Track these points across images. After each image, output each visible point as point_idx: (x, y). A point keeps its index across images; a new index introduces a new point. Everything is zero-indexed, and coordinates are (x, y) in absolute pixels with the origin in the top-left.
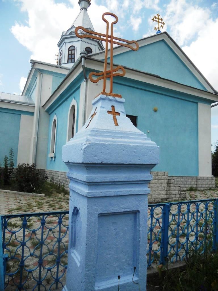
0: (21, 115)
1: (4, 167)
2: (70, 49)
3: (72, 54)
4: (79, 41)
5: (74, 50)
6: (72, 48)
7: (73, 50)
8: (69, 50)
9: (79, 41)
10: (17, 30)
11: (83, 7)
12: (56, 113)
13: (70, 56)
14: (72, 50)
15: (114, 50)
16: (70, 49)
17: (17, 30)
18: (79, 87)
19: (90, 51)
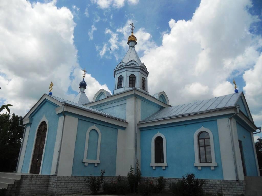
4: (125, 71)
5: (135, 77)
7: (134, 77)
9: (125, 71)
19: (144, 80)
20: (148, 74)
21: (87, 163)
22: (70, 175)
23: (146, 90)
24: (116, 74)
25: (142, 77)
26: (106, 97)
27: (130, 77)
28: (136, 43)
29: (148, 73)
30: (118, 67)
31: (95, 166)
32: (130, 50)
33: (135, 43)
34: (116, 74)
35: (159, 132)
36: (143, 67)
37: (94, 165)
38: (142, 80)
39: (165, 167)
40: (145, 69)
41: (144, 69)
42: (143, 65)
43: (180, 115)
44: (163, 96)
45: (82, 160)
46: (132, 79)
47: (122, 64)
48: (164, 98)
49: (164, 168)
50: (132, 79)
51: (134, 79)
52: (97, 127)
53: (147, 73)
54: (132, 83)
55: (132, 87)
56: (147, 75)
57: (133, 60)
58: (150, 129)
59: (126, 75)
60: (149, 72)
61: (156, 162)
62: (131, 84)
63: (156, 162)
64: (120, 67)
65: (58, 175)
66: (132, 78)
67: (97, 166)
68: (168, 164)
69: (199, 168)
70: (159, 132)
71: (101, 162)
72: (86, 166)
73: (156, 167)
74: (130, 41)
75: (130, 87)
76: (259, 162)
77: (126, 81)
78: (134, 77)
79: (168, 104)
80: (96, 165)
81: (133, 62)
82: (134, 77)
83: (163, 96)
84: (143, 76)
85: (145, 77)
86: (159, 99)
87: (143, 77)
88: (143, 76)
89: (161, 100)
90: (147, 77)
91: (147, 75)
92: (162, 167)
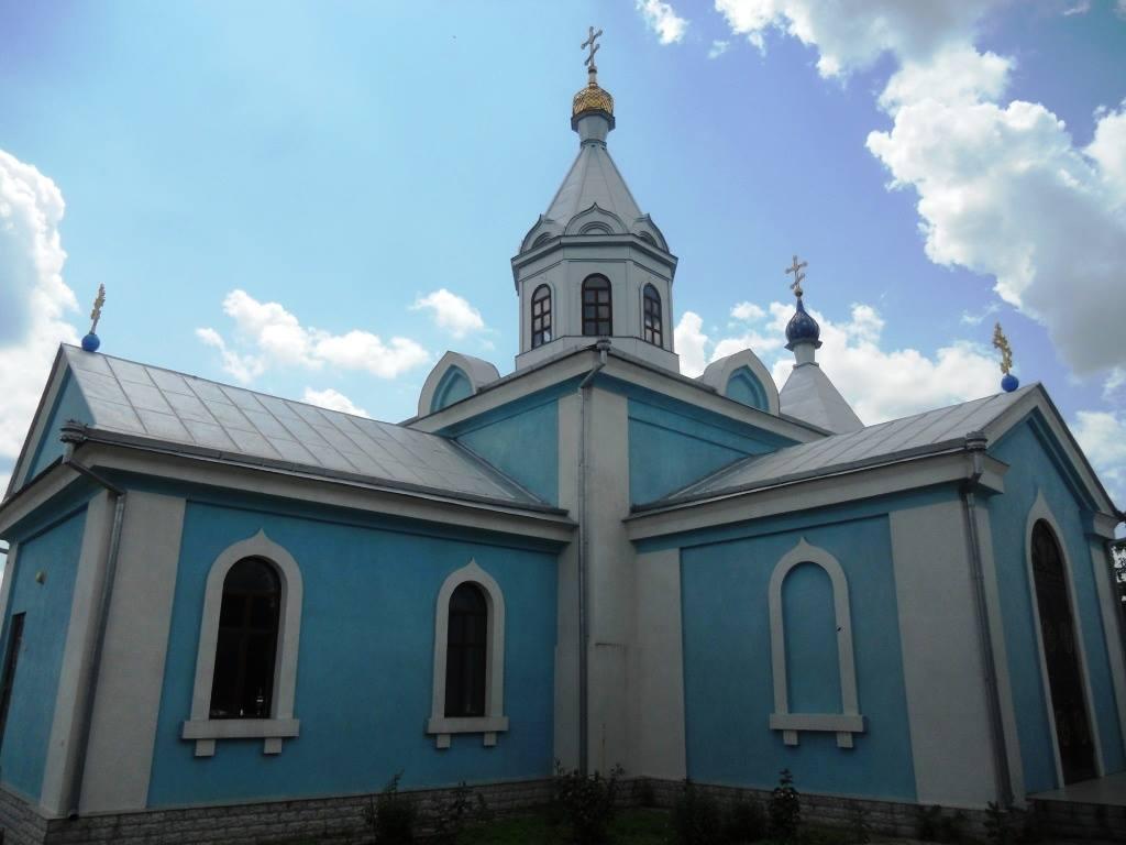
0: (887, 515)
1: (592, 778)
2: (538, 297)
3: (543, 314)
4: (558, 263)
5: (608, 289)
6: (543, 293)
7: (603, 289)
8: (534, 303)
9: (558, 263)
10: (875, 141)
11: (586, 136)
12: (466, 691)
13: (538, 322)
14: (542, 301)
15: (995, 393)
16: (538, 297)
17: (875, 141)
18: (85, 508)
19: (654, 296)
20: (672, 267)
21: (280, 741)
22: (140, 806)
23: (666, 346)
24: (523, 281)
25: (643, 287)
26: (475, 393)
27: (585, 289)
28: (610, 122)
29: (672, 261)
30: (529, 247)
31: (786, 742)
32: (584, 153)
33: (604, 123)
34: (523, 281)
35: (261, 534)
36: (646, 238)
37: (263, 748)
38: (646, 297)
39: (494, 736)
40: (660, 245)
41: (653, 244)
42: (645, 227)
43: (843, 466)
44: (747, 375)
45: (181, 727)
46: (596, 294)
47: (544, 229)
48: (751, 380)
49: (490, 740)
50: (596, 294)
51: (603, 298)
52: (272, 544)
53: (671, 264)
54: (601, 324)
55: (597, 334)
56: (666, 272)
57: (594, 208)
58: (309, 519)
59: (566, 279)
60: (677, 259)
61: (452, 711)
62: (603, 320)
63: (452, 711)
64: (536, 245)
65: (84, 811)
66: (597, 290)
67: (448, 745)
68: (866, 721)
69: (791, 739)
70: (261, 534)
71: (510, 723)
72: (445, 749)
73: (453, 735)
74: (580, 113)
75: (585, 333)
76: (1050, 673)
77: (567, 313)
78: (606, 285)
79: (773, 411)
80: (270, 748)
81: (596, 217)
82: (603, 289)
83: (747, 375)
84: (646, 278)
85: (659, 284)
86: (727, 391)
87: (649, 286)
88: (645, 278)
89: (742, 394)
90: (669, 280)
91: (668, 275)
92: (481, 734)
